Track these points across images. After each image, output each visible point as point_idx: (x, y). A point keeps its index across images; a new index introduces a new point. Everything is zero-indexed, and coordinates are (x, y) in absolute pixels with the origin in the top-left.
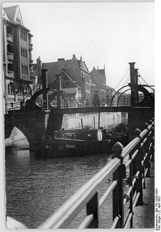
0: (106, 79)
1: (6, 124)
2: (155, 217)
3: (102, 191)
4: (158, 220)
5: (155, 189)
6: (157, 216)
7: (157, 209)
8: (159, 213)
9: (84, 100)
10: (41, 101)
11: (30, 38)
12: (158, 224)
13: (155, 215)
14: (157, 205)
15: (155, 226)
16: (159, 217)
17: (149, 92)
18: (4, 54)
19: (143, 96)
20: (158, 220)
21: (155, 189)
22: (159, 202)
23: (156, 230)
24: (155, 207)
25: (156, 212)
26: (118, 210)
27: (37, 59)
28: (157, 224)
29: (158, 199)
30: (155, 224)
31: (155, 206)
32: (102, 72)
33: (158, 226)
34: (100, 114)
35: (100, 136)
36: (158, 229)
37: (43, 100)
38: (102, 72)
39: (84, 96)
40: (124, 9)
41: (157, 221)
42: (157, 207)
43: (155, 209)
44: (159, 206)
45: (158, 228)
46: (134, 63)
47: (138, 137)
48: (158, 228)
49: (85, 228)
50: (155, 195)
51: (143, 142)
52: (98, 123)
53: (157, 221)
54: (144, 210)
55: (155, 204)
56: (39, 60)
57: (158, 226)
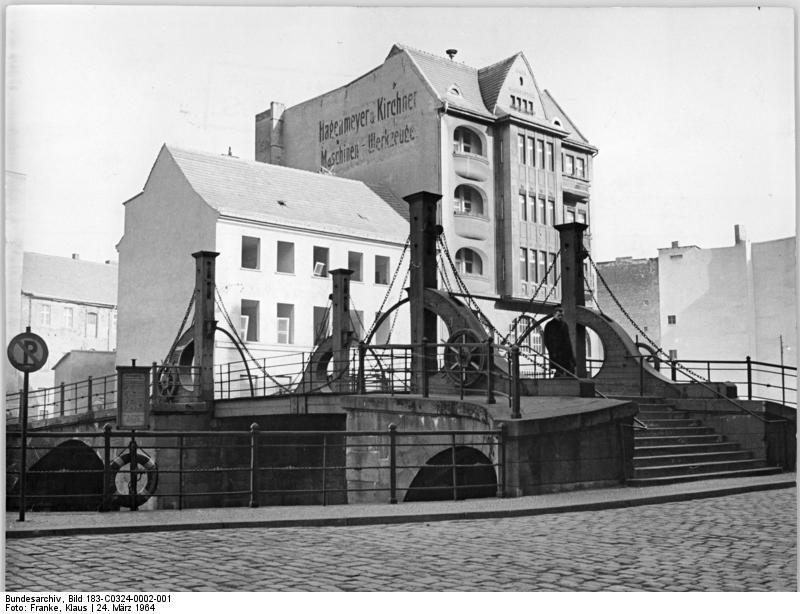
0: (398, 215)
1: (579, 418)
2: (53, 594)
3: (456, 274)
4: (43, 604)
5: (171, 594)
6: (54, 600)
9: (126, 459)
10: (184, 439)
11: (199, 341)
12: (27, 605)
13: (58, 594)
16: (56, 608)
19: (100, 445)
22: (134, 608)
23: (8, 598)
24: (85, 595)
25: (71, 598)
27: (259, 117)
28: (28, 599)
29: (145, 603)
31: (91, 594)
33: (19, 604)
36: (10, 603)
41: (39, 600)
42: (85, 599)
43: (79, 594)
45: (14, 604)
46: (218, 254)
48: (14, 604)
50: (152, 593)
53: (39, 600)
54: (177, 401)
55: (96, 594)
57: (19, 604)
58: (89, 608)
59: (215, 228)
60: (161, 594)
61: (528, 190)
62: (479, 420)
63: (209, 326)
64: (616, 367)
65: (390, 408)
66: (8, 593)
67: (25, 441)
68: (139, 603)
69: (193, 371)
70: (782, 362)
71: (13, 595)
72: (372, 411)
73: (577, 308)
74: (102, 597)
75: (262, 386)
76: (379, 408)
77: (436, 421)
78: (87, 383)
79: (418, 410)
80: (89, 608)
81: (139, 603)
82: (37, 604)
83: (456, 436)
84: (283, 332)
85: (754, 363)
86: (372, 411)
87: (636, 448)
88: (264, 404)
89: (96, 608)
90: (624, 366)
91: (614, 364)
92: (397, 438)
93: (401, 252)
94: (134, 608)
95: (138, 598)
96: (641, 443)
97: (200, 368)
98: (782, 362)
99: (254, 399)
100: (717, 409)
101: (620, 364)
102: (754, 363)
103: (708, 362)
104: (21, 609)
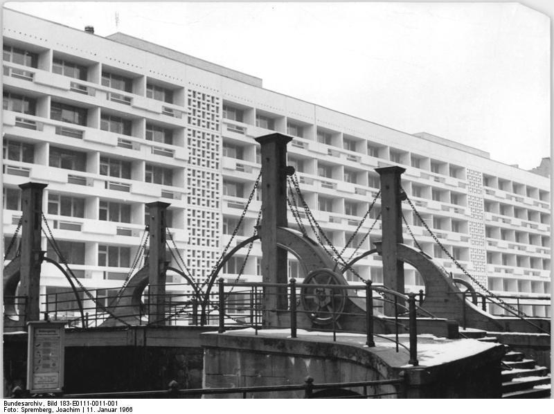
2: (36, 400)
4: (30, 407)
6: (37, 404)
7: (56, 404)
8: (86, 410)
12: (19, 408)
13: (40, 400)
14: (64, 404)
15: (14, 400)
18: (276, 393)
20: (30, 407)
21: (115, 400)
23: (5, 403)
24: (59, 400)
25: (49, 404)
28: (19, 404)
30: (321, 285)
31: (63, 400)
32: (57, 133)
33: (13, 407)
35: (402, 192)
36: (7, 406)
38: (57, 133)
40: (81, 17)
41: (27, 404)
42: (59, 404)
43: (55, 400)
45: (10, 407)
48: (10, 407)
49: (3, 184)
51: (425, 295)
53: (27, 404)
55: (66, 400)
57: (13, 407)
61: (51, 348)
62: (360, 364)
63: (37, 257)
64: (438, 302)
65: (257, 349)
66: (5, 400)
69: (16, 301)
71: (9, 401)
72: (234, 350)
73: (397, 245)
74: (106, 402)
76: (244, 348)
77: (308, 363)
79: (289, 351)
80: (81, 410)
83: (368, 388)
84: (23, 120)
86: (234, 350)
87: (504, 384)
88: (97, 335)
89: (86, 410)
90: (446, 301)
91: (435, 299)
94: (118, 410)
96: (510, 377)
97: (26, 298)
99: (86, 330)
100: (541, 345)
101: (442, 299)
103: (518, 298)
104: (15, 410)
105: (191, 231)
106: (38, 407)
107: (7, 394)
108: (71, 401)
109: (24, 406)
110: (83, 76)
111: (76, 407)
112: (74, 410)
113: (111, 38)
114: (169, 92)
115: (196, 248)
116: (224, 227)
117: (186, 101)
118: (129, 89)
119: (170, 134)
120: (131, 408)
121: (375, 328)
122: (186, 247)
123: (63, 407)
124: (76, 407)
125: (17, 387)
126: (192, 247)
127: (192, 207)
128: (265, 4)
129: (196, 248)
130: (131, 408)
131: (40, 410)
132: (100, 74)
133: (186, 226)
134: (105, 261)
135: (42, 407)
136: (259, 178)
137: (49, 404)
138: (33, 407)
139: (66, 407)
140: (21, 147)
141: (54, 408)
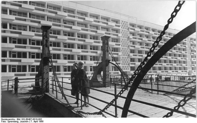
2: (13, 118)
4: (11, 120)
7: (20, 119)
8: (31, 121)
12: (7, 121)
13: (14, 118)
14: (23, 119)
15: (5, 118)
17: (175, 112)
20: (11, 120)
22: (38, 121)
23: (2, 119)
24: (21, 118)
25: (17, 119)
26: (82, 83)
28: (7, 119)
29: (41, 120)
30: (7, 118)
31: (22, 118)
33: (5, 121)
34: (19, 87)
36: (3, 120)
37: (67, 45)
39: (113, 80)
41: (10, 120)
42: (21, 119)
43: (19, 118)
44: (35, 122)
45: (3, 121)
47: (115, 107)
48: (3, 121)
52: (168, 86)
53: (10, 120)
55: (24, 118)
56: (107, 59)
57: (5, 121)
58: (29, 121)
59: (34, 76)
60: (34, 118)
67: (125, 82)
68: (40, 120)
70: (152, 88)
71: (3, 118)
75: (159, 84)
78: (7, 82)
80: (29, 121)
81: (40, 120)
82: (9, 120)
85: (60, 82)
89: (31, 121)
92: (63, 87)
93: (62, 79)
94: (38, 121)
95: (40, 119)
98: (152, 88)
102: (60, 82)
103: (175, 76)
105: (122, 53)
106: (14, 121)
107: (3, 116)
108: (25, 118)
109: (9, 120)
110: (107, 31)
111: (27, 121)
112: (26, 122)
113: (175, 92)
114: (117, 21)
115: (124, 56)
116: (130, 51)
117: (121, 23)
118: (117, 32)
119: (117, 31)
120: (43, 121)
121: (52, 62)
122: (121, 56)
123: (22, 121)
124: (27, 121)
125: (6, 113)
126: (123, 56)
127: (122, 47)
128: (160, 105)
129: (124, 56)
130: (43, 121)
131: (14, 122)
132: (100, 18)
133: (121, 52)
134: (83, 58)
135: (15, 121)
136: (140, 86)
137: (17, 119)
138: (12, 121)
139: (24, 121)
140: (22, 14)
141: (19, 121)
